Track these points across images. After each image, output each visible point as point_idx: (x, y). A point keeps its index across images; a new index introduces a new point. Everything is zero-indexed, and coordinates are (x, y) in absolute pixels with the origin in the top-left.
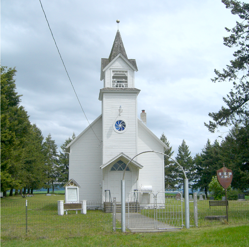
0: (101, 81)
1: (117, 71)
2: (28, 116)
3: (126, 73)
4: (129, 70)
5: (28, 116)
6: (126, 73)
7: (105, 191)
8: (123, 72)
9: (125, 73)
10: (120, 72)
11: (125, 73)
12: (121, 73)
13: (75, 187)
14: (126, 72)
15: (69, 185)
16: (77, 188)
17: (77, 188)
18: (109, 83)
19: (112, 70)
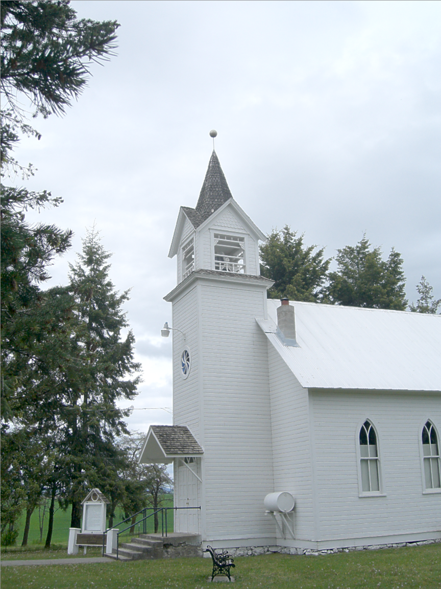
0: (171, 257)
1: (222, 237)
2: (385, 258)
3: (241, 243)
4: (247, 236)
5: (385, 258)
6: (241, 243)
7: (207, 510)
8: (235, 238)
9: (238, 242)
10: (229, 238)
11: (238, 242)
12: (225, 240)
13: (100, 504)
14: (242, 239)
15: (89, 499)
16: (87, 506)
17: (87, 506)
18: (205, 259)
19: (213, 233)
